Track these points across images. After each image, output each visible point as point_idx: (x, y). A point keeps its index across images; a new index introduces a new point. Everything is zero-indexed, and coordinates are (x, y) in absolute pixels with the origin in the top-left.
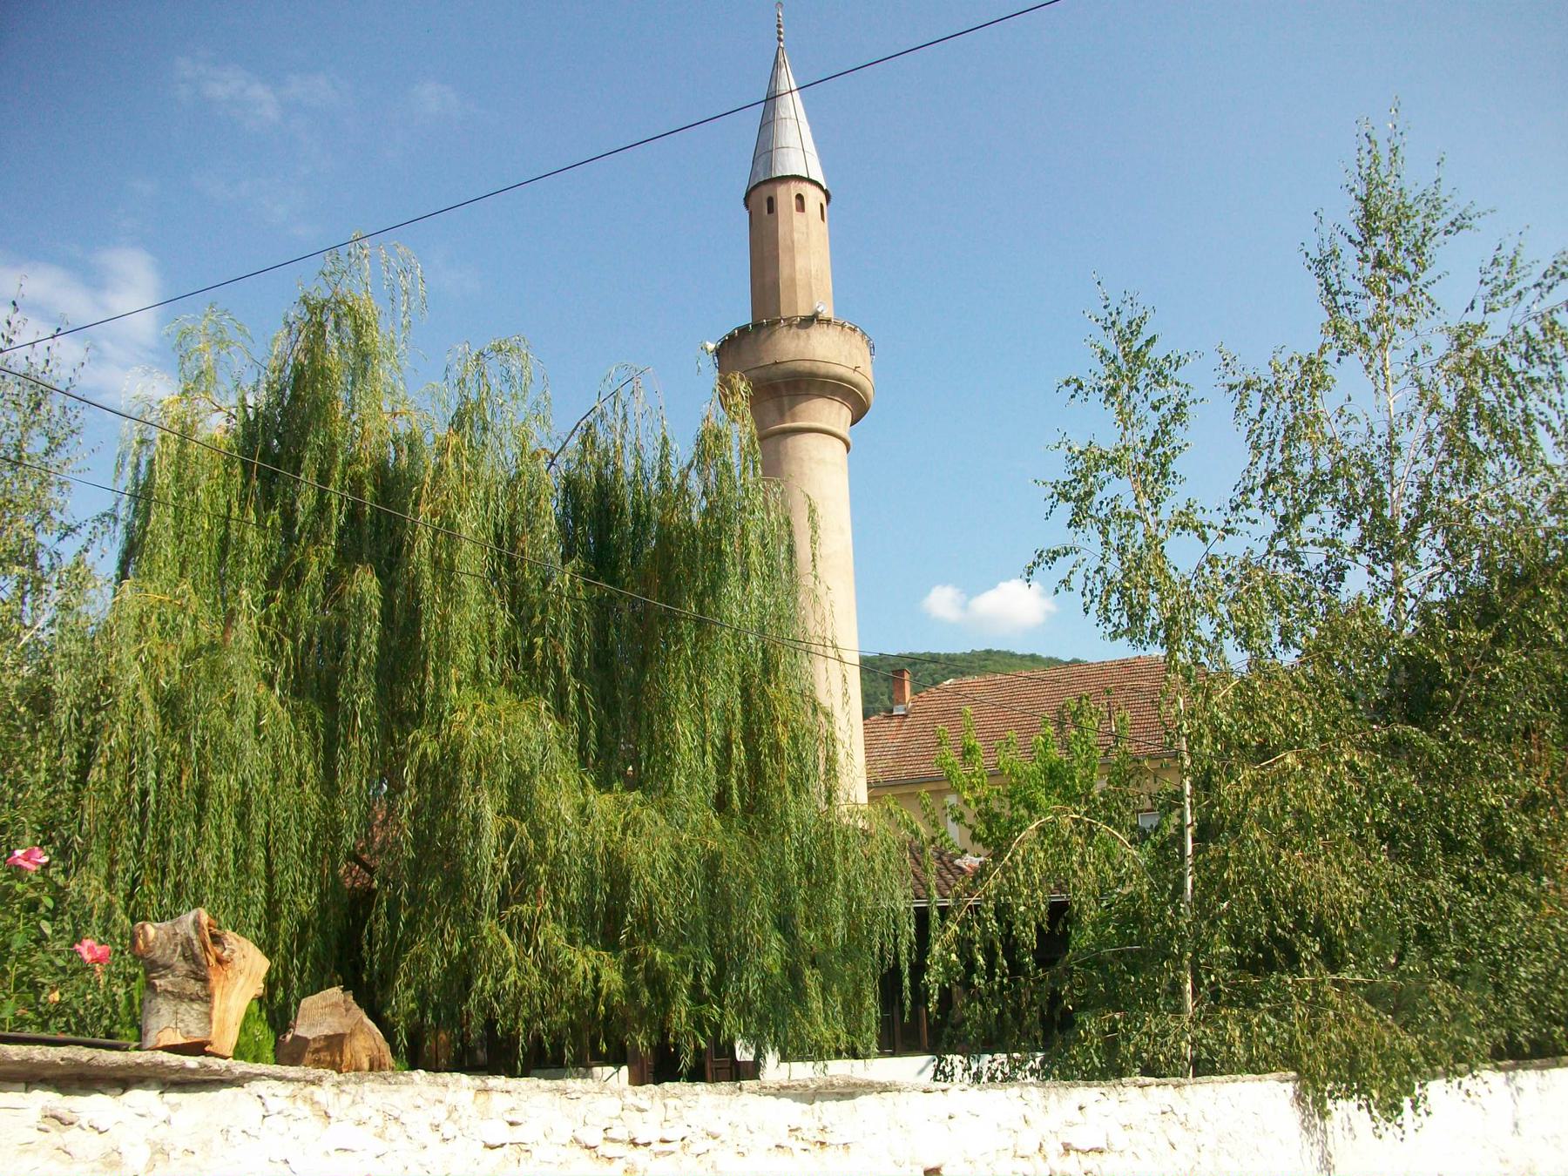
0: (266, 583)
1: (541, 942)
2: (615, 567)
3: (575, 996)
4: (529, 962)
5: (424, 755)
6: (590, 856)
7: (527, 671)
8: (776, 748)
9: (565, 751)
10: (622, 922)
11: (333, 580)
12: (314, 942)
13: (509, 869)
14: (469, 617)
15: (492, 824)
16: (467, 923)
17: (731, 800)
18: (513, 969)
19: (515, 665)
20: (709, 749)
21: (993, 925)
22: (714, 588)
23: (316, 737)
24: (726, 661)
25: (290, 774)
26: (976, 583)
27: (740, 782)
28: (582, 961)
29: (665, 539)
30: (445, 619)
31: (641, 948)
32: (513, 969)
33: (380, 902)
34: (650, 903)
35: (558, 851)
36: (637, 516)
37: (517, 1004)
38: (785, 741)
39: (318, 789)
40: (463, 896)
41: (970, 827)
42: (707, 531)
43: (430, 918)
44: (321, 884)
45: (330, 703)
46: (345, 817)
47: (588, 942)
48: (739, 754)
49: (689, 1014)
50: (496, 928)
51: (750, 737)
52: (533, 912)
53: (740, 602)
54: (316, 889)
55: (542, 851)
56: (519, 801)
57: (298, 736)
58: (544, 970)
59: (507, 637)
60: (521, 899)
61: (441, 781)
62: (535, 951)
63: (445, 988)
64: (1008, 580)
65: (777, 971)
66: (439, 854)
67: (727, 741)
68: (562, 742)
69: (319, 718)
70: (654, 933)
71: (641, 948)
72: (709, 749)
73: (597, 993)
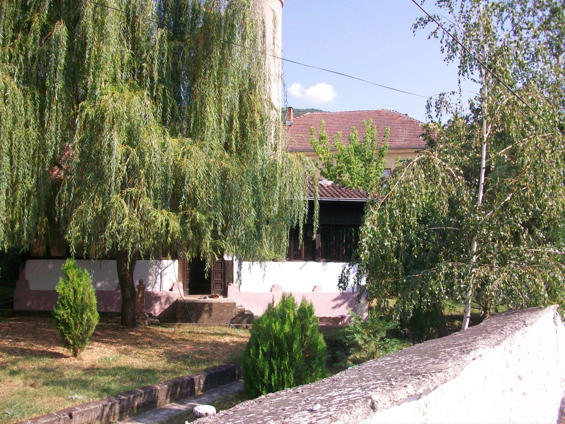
0: (13, 30)
1: (141, 207)
2: (183, 33)
3: (157, 233)
4: (135, 215)
5: (87, 115)
6: (166, 167)
7: (138, 78)
8: (253, 124)
9: (156, 117)
10: (180, 199)
11: (46, 30)
12: (34, 201)
13: (127, 170)
14: (111, 50)
15: (118, 149)
16: (105, 195)
17: (231, 146)
18: (127, 219)
19: (133, 76)
20: (223, 120)
21: (397, 213)
22: (229, 42)
23: (35, 104)
24: (233, 81)
25: (22, 120)
26: (307, 84)
27: (236, 138)
28: (161, 216)
29: (207, 20)
30: (99, 49)
31: (189, 211)
32: (127, 219)
33: (64, 184)
34: (194, 190)
35: (151, 163)
36: (194, 10)
37: (128, 235)
38: (258, 121)
39: (36, 130)
40: (104, 183)
41: (320, 169)
42: (227, 16)
43: (88, 192)
44: (37, 175)
45: (43, 88)
46: (49, 143)
47: (163, 207)
48: (236, 124)
49: (211, 243)
50: (119, 199)
51: (242, 117)
52: (138, 192)
53: (239, 58)
54: (35, 176)
55: (143, 162)
56: (132, 138)
57: (26, 103)
58: (142, 220)
59: (129, 62)
60: (133, 185)
61: (95, 127)
62: (138, 210)
63: (95, 226)
64: (320, 83)
65: (252, 225)
66: (93, 162)
67: (231, 117)
68: (155, 114)
69: (37, 96)
70: (195, 205)
71: (189, 211)
72: (223, 120)
73: (167, 232)
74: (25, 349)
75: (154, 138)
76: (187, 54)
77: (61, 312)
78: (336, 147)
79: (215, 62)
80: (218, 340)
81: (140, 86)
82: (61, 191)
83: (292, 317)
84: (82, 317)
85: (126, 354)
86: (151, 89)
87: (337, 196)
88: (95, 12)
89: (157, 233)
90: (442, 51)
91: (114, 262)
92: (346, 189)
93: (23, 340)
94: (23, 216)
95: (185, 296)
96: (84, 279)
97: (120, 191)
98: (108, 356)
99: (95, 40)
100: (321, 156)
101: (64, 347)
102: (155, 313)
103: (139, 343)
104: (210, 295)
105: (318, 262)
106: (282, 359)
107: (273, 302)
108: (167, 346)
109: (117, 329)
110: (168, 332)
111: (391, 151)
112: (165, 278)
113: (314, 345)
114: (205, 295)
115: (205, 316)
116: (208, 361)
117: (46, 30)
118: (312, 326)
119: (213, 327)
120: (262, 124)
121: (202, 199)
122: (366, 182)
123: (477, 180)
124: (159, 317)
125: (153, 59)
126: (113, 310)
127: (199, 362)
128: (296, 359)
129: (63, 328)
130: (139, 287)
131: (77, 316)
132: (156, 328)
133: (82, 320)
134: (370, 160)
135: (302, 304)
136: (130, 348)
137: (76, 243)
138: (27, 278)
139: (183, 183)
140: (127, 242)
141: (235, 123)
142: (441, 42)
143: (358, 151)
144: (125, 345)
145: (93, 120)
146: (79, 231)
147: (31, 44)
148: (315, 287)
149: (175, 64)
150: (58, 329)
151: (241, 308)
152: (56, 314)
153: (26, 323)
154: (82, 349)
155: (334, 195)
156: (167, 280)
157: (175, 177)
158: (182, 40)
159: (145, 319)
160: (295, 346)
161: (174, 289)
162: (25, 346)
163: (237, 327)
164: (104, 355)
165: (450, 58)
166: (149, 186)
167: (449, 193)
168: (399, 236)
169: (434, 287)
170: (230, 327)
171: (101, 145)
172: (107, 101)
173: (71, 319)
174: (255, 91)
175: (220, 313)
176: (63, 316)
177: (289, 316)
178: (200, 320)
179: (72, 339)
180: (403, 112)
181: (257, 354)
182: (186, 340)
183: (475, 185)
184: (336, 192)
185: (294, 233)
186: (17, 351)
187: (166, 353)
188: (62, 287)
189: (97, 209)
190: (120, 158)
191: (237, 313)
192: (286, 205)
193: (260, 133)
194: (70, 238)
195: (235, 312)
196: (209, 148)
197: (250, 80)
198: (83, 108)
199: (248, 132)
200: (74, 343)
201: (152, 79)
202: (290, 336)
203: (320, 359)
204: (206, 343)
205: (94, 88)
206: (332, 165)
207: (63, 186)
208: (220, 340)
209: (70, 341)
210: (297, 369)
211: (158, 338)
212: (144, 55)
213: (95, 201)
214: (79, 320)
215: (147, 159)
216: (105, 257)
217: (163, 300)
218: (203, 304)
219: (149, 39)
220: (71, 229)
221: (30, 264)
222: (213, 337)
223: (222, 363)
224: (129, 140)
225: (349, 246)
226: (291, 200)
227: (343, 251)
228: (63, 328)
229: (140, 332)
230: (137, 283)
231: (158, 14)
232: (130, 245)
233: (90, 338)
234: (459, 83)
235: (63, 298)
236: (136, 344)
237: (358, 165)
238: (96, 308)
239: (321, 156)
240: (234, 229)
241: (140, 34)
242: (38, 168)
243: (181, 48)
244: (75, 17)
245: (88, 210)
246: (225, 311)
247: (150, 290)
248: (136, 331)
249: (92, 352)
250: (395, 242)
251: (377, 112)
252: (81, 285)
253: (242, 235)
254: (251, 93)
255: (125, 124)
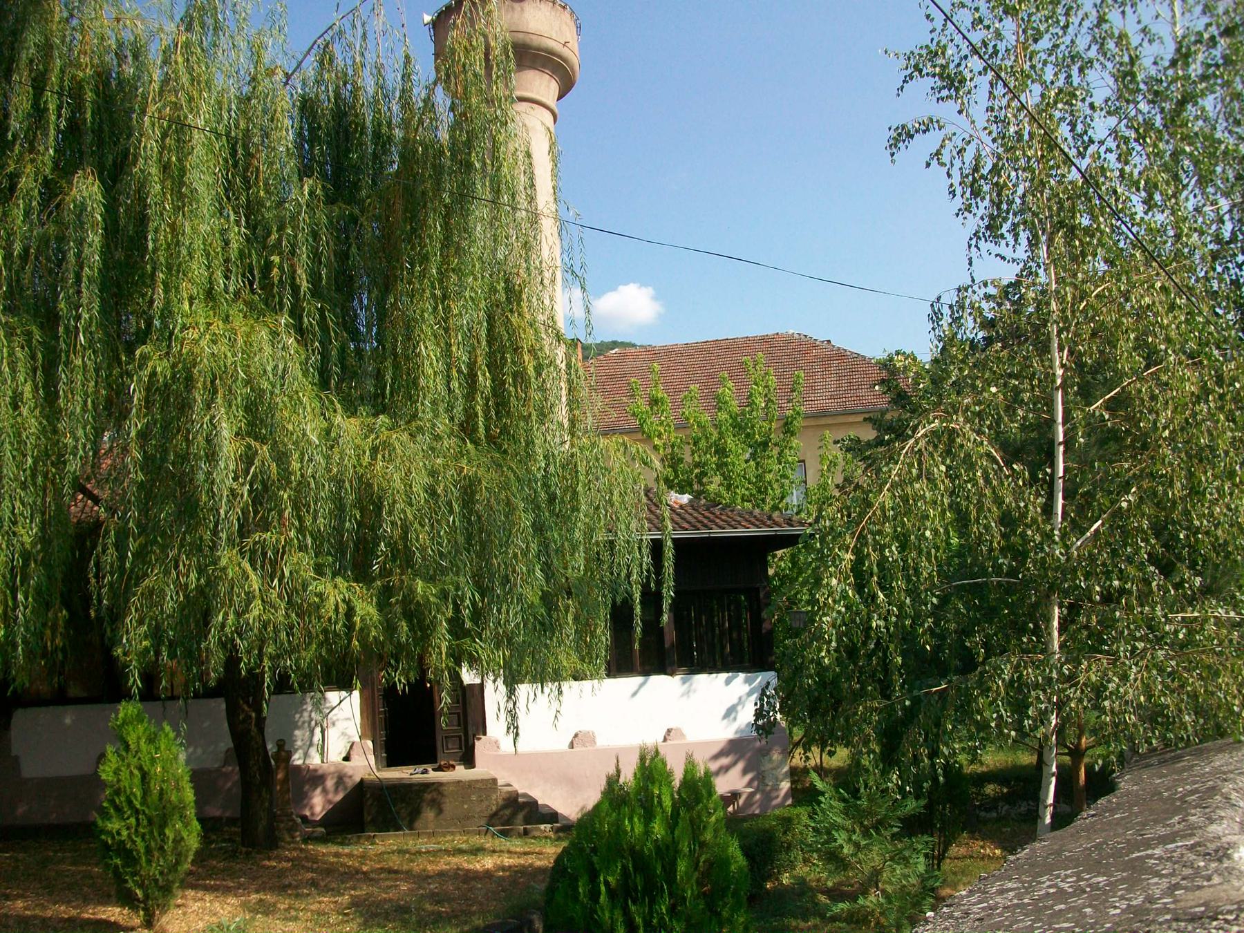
1: (287, 573)
2: (356, 186)
4: (274, 595)
5: (154, 374)
6: (339, 482)
7: (264, 290)
8: (520, 377)
11: (51, 191)
12: (36, 576)
13: (250, 492)
14: (201, 229)
15: (229, 448)
16: (205, 554)
19: (251, 284)
20: (454, 373)
23: (33, 357)
24: (475, 285)
28: (334, 592)
29: (407, 157)
31: (395, 579)
33: (107, 532)
36: (377, 135)
38: (531, 372)
39: (37, 412)
40: (198, 524)
43: (164, 548)
44: (43, 513)
45: (49, 319)
46: (69, 441)
48: (484, 380)
49: (450, 647)
51: (495, 366)
55: (285, 473)
56: (258, 420)
57: (11, 354)
60: (266, 526)
61: (173, 399)
62: (280, 581)
65: (537, 601)
67: (472, 366)
70: (408, 562)
72: (454, 373)
73: (350, 626)
74: (29, 917)
75: (306, 419)
76: (371, 230)
77: (114, 825)
78: (687, 419)
79: (433, 247)
80: (466, 865)
81: (266, 304)
82: (100, 548)
83: (667, 803)
84: (162, 834)
85: (266, 913)
86: (296, 313)
87: (706, 526)
88: (163, 147)
89: (325, 631)
90: (953, 193)
91: (221, 705)
92: (722, 509)
93: (18, 897)
94: (14, 609)
95: (378, 770)
96: (163, 747)
97: (238, 540)
98: (224, 920)
99: (164, 208)
100: (657, 441)
101: (123, 906)
102: (313, 814)
103: (290, 886)
104: (436, 766)
105: (672, 674)
106: (653, 902)
107: (618, 771)
108: (354, 888)
109: (232, 855)
110: (350, 855)
111: (812, 422)
112: (332, 733)
113: (720, 863)
114: (425, 766)
115: (429, 814)
116: (456, 917)
117: (51, 191)
118: (713, 819)
119: (449, 838)
120: (540, 375)
121: (423, 549)
122: (760, 492)
123: (1048, 470)
124: (327, 821)
125: (293, 247)
126: (217, 813)
127: (435, 922)
128: (684, 899)
129: (118, 862)
130: (277, 757)
131: (151, 832)
132: (322, 849)
133: (163, 840)
134: (765, 445)
135: (686, 772)
136: (269, 898)
137: (140, 664)
138: (14, 752)
139: (379, 514)
140: (261, 655)
141: (480, 378)
142: (949, 175)
143: (740, 427)
144: (257, 892)
145: (166, 385)
146: (146, 637)
147: (19, 222)
148: (669, 731)
149: (343, 256)
150: (107, 866)
151: (509, 789)
152: (102, 831)
153: (21, 856)
154: (164, 909)
155: (699, 525)
156: (337, 735)
157: (360, 504)
158: (351, 200)
159: (291, 830)
160: (682, 866)
161: (354, 756)
162: (26, 909)
163: (505, 833)
164: (214, 919)
165: (968, 209)
166: (301, 525)
167: (999, 501)
168: (901, 607)
169: (987, 714)
170: (489, 835)
171: (187, 439)
172: (196, 342)
173: (138, 840)
174: (519, 305)
175: (463, 803)
176: (119, 833)
177: (660, 803)
178: (417, 824)
179: (141, 886)
180: (820, 336)
181: (594, 895)
182: (396, 872)
183: (1044, 480)
184: (701, 518)
185: (620, 616)
186: (11, 922)
187: (355, 903)
188: (114, 766)
189: (186, 585)
190: (232, 466)
191: (501, 802)
192: (598, 553)
193: (536, 396)
194: (125, 654)
195: (496, 800)
196: (427, 437)
197: (507, 281)
198: (145, 358)
199: (510, 395)
200: (147, 897)
201: (296, 289)
202: (667, 847)
203: (735, 894)
204: (441, 874)
205: (167, 313)
206: (681, 460)
207: (104, 537)
208: (471, 867)
209: (138, 891)
210: (688, 921)
211: (329, 871)
212: (274, 236)
213: (181, 567)
214: (155, 841)
215: (295, 466)
216: (211, 693)
217: (330, 783)
218: (427, 786)
219: (280, 204)
220: (127, 632)
221: (22, 719)
222: (455, 860)
223: (491, 919)
224: (251, 424)
225: (735, 635)
226: (611, 542)
227: (723, 648)
228: (118, 862)
229: (289, 860)
230: (271, 747)
231: (299, 147)
232: (267, 663)
233: (182, 881)
234: (970, 264)
235: (118, 792)
236: (282, 889)
237: (740, 456)
238: (193, 811)
239: (657, 441)
240: (499, 611)
241: (262, 193)
242: (44, 498)
243: (354, 220)
244: (115, 162)
245: (168, 588)
246: (474, 798)
247: (299, 762)
248: (280, 859)
249: (184, 914)
250: (894, 619)
251: (765, 339)
252: (158, 758)
253: (518, 625)
254: (511, 311)
255: (242, 391)
